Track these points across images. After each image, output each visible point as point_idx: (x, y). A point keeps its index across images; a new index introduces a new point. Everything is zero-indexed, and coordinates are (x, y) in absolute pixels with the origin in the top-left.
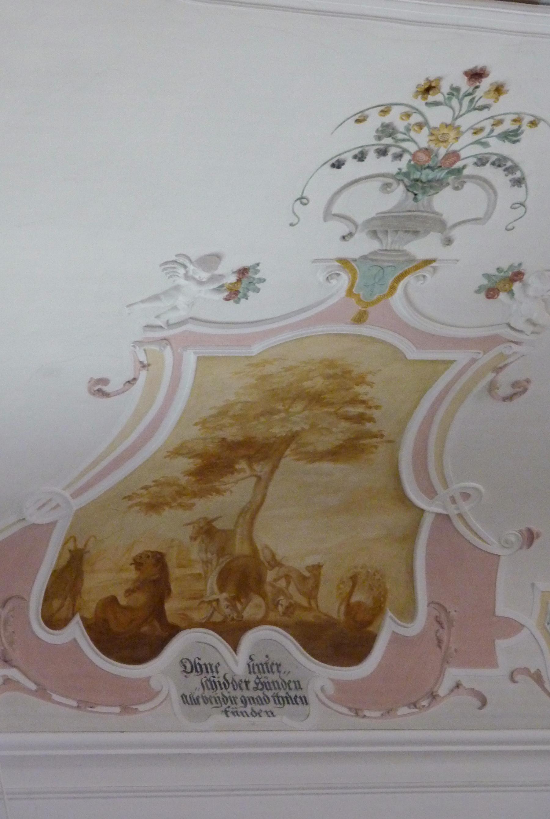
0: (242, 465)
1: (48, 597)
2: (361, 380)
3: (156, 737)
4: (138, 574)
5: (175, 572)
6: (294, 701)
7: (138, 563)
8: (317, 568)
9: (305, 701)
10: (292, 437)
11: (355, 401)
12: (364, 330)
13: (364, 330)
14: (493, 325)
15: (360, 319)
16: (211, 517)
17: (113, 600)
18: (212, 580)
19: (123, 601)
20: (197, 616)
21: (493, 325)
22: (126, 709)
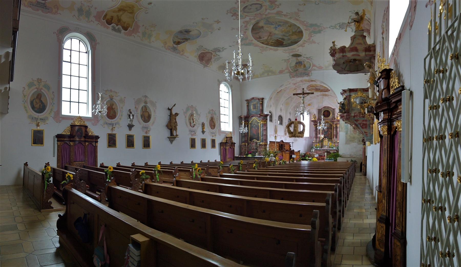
0: (122, 11)
1: (103, 17)
2: (134, 7)
4: (374, 233)
5: (114, 18)
7: (111, 16)
8: (125, 22)
9: (121, 32)
10: (127, 10)
11: (133, 9)
12: (136, 3)
13: (136, 3)
14: (343, 244)
15: (136, 2)
17: (108, 19)
18: (117, 20)
19: (109, 19)
20: (115, 23)
21: (343, 244)
22: (107, 29)
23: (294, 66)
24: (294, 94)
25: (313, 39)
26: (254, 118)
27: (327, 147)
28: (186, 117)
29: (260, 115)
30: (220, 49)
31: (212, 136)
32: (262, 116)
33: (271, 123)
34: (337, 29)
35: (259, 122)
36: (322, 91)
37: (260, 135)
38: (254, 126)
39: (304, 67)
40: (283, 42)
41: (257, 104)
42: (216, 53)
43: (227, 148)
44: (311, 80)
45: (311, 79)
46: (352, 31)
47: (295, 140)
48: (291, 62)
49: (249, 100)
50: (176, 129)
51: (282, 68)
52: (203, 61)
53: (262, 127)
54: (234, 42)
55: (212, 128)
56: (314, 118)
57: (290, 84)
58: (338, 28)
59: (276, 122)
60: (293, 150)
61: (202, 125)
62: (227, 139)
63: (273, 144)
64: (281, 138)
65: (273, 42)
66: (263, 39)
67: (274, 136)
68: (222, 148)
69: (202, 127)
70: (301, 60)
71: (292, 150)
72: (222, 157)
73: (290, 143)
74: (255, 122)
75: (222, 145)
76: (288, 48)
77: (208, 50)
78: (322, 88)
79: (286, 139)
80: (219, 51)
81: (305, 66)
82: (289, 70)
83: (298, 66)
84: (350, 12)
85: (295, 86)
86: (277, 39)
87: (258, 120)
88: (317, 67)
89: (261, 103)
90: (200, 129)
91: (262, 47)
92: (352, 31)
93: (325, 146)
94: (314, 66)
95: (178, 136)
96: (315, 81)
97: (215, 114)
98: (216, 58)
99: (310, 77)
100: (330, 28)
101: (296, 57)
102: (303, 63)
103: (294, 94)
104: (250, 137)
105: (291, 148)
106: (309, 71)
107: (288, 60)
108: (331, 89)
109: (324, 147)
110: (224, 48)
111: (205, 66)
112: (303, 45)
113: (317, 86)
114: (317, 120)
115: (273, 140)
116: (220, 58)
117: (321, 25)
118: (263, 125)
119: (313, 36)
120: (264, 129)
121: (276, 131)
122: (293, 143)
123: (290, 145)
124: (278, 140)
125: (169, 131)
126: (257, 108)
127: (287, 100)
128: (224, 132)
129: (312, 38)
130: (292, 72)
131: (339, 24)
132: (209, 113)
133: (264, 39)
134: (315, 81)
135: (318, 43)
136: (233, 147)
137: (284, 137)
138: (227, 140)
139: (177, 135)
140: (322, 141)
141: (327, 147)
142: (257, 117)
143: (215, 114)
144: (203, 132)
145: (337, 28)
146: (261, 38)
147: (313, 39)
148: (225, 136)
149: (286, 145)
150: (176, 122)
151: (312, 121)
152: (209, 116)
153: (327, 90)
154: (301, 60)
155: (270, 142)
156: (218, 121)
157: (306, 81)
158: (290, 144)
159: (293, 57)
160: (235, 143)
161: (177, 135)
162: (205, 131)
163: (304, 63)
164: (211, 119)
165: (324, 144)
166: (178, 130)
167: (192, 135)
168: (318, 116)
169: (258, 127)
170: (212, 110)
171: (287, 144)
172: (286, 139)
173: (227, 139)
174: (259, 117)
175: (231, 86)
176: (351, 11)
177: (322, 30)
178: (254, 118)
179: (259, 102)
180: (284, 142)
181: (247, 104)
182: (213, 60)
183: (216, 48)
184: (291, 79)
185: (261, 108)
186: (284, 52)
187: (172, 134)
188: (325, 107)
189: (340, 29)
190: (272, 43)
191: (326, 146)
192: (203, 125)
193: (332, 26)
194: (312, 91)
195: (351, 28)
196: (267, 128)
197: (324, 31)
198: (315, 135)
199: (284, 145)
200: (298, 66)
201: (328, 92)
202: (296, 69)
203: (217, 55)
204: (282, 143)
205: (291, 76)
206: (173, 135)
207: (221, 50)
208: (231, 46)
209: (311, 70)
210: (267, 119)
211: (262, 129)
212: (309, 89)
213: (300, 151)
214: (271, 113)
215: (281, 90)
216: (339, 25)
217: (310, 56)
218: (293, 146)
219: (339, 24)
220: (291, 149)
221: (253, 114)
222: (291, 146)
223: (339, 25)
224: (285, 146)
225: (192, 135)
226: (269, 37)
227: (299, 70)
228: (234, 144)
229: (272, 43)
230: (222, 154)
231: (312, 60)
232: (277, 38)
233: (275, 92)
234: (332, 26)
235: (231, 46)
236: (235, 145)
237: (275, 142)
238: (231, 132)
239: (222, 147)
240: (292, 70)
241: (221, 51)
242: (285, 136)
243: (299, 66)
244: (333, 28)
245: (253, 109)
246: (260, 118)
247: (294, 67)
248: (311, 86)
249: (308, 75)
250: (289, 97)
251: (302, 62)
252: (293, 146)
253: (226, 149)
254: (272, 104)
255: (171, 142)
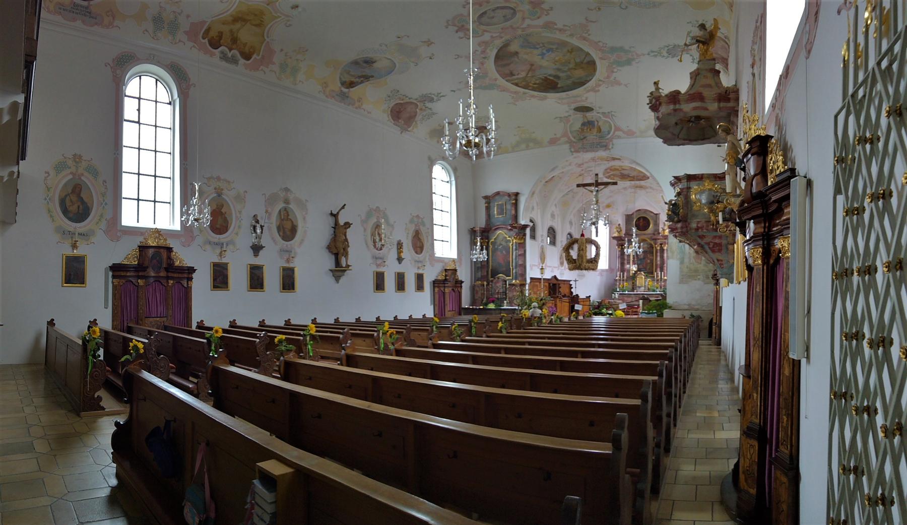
0: (240, 22)
1: (203, 34)
2: (264, 15)
3: (789, 431)
5: (223, 36)
6: (236, 63)
7: (219, 32)
8: (246, 43)
9: (238, 64)
10: (250, 20)
11: (262, 18)
12: (267, 7)
13: (267, 7)
14: (675, 479)
15: (268, 5)
16: (472, 228)
17: (213, 37)
18: (230, 40)
19: (215, 37)
20: (226, 44)
21: (675, 479)
23: (578, 129)
24: (578, 186)
25: (615, 78)
26: (500, 232)
27: (643, 288)
28: (365, 230)
29: (511, 225)
30: (433, 96)
31: (417, 268)
32: (515, 228)
33: (533, 242)
34: (663, 56)
35: (509, 241)
36: (633, 179)
37: (512, 266)
38: (500, 247)
39: (597, 132)
40: (558, 84)
41: (506, 205)
42: (425, 105)
43: (447, 290)
44: (613, 158)
45: (611, 155)
46: (692, 61)
47: (579, 276)
48: (572, 122)
49: (490, 196)
50: (346, 254)
51: (555, 135)
52: (400, 121)
53: (516, 250)
54: (460, 83)
55: (416, 253)
56: (618, 231)
57: (570, 165)
58: (666, 55)
59: (542, 240)
60: (577, 295)
61: (398, 247)
62: (447, 273)
63: (538, 283)
64: (552, 271)
65: (537, 82)
66: (518, 76)
67: (538, 268)
68: (436, 291)
69: (398, 249)
70: (592, 118)
71: (574, 294)
72: (437, 308)
73: (571, 281)
74: (502, 240)
75: (436, 285)
76: (567, 95)
77: (410, 99)
78: (633, 174)
79: (562, 274)
80: (431, 100)
81: (599, 130)
82: (569, 138)
83: (587, 129)
84: (688, 23)
85: (580, 169)
86: (545, 77)
87: (507, 236)
88: (624, 132)
89: (513, 203)
90: (393, 254)
91: (515, 92)
92: (692, 61)
93: (639, 287)
94: (618, 129)
95: (350, 268)
96: (619, 159)
97: (423, 224)
98: (425, 113)
99: (610, 152)
100: (649, 54)
101: (583, 112)
102: (596, 123)
103: (578, 186)
104: (491, 270)
105: (572, 290)
106: (607, 139)
107: (567, 117)
108: (652, 176)
109: (637, 288)
110: (440, 94)
111: (404, 130)
112: (597, 89)
113: (624, 169)
114: (623, 236)
115: (538, 275)
116: (434, 114)
117: (632, 49)
118: (517, 246)
119: (615, 70)
120: (520, 253)
121: (543, 258)
122: (576, 281)
123: (571, 285)
124: (548, 275)
125: (333, 257)
126: (505, 211)
127: (564, 196)
128: (441, 260)
129: (614, 75)
130: (574, 142)
131: (667, 47)
132: (411, 221)
133: (520, 76)
134: (619, 159)
135: (626, 85)
136: (459, 289)
137: (558, 269)
138: (446, 276)
139: (348, 266)
140: (634, 277)
141: (643, 288)
142: (506, 231)
143: (424, 225)
144: (400, 260)
145: (662, 55)
146: (514, 75)
147: (615, 78)
148: (444, 267)
149: (563, 285)
150: (346, 240)
151: (614, 238)
152: (412, 228)
153: (644, 178)
154: (592, 118)
155: (531, 279)
156: (430, 238)
157: (602, 159)
158: (571, 283)
159: (576, 112)
160: (463, 282)
161: (348, 266)
162: (403, 257)
163: (598, 124)
164: (414, 234)
165: (638, 284)
166: (349, 256)
167: (378, 266)
168: (626, 227)
169: (507, 249)
170: (418, 216)
171: (565, 283)
172: (562, 274)
173: (447, 273)
174: (510, 229)
175: (455, 170)
176: (691, 22)
177: (633, 59)
178: (500, 232)
179: (510, 200)
180: (559, 278)
181: (486, 205)
182: (418, 118)
183: (426, 94)
184: (573, 155)
185: (513, 212)
186: (559, 103)
187: (338, 263)
188: (639, 210)
189: (669, 57)
190: (535, 84)
191: (642, 286)
192: (400, 245)
193: (653, 52)
194: (613, 180)
195: (691, 56)
196: (525, 251)
197: (637, 60)
198: (620, 266)
199: (559, 284)
200: (587, 129)
201: (645, 181)
202: (583, 136)
203: (427, 107)
204: (555, 282)
205: (572, 150)
206: (341, 265)
207: (435, 98)
208: (454, 91)
209: (612, 138)
210: (525, 235)
211: (516, 253)
212: (608, 175)
213: (591, 298)
214: (533, 222)
215: (554, 176)
216: (668, 50)
217: (609, 111)
218: (576, 288)
219: (667, 47)
220: (572, 293)
221: (498, 224)
222: (572, 288)
223: (666, 49)
224: (560, 287)
225: (378, 266)
226: (530, 73)
227: (588, 137)
228: (461, 284)
229: (535, 84)
230: (437, 303)
231: (614, 117)
232: (545, 76)
233: (541, 181)
234: (653, 52)
235: (454, 91)
236: (463, 285)
237: (540, 279)
238: (454, 260)
239: (436, 289)
240: (574, 138)
241: (435, 100)
242: (560, 267)
243: (589, 130)
244: (656, 56)
245: (499, 214)
246: (512, 232)
247: (578, 131)
248: (611, 169)
249: (606, 147)
250: (569, 191)
251: (594, 121)
252: (576, 288)
253: (444, 293)
254: (535, 205)
255: (337, 279)
